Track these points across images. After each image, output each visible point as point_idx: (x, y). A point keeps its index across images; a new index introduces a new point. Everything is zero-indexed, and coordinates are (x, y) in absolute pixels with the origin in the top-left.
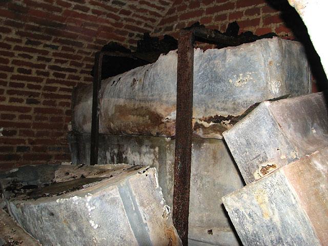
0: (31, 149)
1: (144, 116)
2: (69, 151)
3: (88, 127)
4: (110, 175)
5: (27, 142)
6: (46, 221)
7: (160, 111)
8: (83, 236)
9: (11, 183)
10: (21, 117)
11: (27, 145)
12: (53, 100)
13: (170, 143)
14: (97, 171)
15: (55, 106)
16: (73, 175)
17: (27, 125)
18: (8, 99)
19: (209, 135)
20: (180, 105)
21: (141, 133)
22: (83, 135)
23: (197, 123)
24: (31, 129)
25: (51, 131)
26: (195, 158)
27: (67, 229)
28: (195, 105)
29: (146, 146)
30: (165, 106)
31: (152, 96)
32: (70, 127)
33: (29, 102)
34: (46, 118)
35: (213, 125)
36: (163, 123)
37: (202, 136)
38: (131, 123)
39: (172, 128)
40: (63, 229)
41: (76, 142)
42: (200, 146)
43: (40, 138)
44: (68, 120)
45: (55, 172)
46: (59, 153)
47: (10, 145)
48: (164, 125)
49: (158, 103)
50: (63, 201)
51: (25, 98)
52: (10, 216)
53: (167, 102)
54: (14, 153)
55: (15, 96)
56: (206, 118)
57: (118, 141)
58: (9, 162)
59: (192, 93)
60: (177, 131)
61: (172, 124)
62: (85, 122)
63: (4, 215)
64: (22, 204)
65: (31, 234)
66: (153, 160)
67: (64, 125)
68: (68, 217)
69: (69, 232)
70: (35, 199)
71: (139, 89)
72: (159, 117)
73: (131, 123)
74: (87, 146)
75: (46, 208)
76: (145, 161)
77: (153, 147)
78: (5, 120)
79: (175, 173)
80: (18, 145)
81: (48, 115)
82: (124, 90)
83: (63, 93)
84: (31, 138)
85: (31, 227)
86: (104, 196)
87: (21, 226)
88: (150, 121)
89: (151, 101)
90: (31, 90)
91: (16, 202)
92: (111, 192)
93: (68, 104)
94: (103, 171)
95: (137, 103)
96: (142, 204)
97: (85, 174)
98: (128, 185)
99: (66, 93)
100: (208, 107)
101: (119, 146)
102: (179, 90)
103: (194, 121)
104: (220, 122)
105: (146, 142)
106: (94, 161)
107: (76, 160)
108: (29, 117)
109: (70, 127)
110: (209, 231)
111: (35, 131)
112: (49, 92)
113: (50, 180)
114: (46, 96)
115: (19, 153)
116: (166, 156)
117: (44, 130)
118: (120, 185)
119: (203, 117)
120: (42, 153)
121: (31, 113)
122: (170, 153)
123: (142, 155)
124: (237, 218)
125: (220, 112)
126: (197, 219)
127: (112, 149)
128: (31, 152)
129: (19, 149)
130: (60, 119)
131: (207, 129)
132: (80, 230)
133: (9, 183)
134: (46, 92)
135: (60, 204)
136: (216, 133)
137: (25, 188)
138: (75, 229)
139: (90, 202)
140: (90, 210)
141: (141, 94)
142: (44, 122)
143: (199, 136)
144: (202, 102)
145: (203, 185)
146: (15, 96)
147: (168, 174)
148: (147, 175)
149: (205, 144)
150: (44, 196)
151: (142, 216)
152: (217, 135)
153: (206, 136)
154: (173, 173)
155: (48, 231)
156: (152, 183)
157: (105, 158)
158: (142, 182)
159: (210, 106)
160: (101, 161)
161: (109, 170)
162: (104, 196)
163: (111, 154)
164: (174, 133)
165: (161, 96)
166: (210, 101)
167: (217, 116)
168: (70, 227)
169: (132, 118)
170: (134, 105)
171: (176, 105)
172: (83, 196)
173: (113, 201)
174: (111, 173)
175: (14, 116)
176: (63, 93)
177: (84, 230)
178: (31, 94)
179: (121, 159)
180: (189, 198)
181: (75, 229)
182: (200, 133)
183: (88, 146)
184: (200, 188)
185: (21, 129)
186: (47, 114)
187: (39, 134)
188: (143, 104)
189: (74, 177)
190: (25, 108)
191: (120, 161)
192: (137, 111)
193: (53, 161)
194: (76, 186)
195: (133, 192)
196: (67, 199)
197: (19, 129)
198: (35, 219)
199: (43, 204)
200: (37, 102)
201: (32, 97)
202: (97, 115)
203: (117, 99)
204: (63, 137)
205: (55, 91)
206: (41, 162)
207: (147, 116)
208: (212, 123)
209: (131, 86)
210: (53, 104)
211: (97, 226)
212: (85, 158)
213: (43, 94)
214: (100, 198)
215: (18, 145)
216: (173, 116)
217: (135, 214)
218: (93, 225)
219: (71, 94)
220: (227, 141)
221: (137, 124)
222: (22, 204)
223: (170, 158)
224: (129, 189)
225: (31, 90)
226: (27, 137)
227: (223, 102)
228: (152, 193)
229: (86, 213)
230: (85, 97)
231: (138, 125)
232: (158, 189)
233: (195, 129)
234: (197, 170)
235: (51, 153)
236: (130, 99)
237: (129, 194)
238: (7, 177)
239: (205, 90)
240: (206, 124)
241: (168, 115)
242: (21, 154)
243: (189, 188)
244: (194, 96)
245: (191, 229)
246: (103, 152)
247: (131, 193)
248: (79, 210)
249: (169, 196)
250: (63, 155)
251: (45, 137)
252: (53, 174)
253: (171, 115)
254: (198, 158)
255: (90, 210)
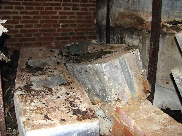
0: (76, 34)
1: (134, 19)
2: (95, 34)
3: (105, 23)
4: (116, 51)
5: (74, 30)
6: (84, 74)
7: (143, 16)
8: (101, 82)
9: (67, 53)
10: (70, 17)
11: (74, 32)
12: (86, 7)
13: (148, 34)
14: (109, 47)
15: (87, 10)
16: (97, 49)
17: (73, 22)
18: (63, 8)
19: (169, 31)
20: (154, 14)
21: (132, 28)
22: (102, 26)
23: (163, 24)
24: (76, 23)
25: (86, 24)
26: (161, 43)
27: (94, 79)
28: (163, 14)
29: (135, 35)
30: (145, 14)
31: (139, 8)
32: (95, 22)
33: (74, 9)
34: (83, 18)
35: (172, 26)
36: (144, 23)
37: (166, 32)
38: (127, 23)
39: (149, 26)
40: (92, 78)
41: (98, 30)
42: (164, 37)
43: (80, 28)
44: (94, 18)
45: (88, 47)
46: (90, 36)
47: (66, 32)
48: (145, 24)
49: (142, 12)
50: (91, 65)
51: (71, 7)
52: (67, 69)
53: (147, 12)
54: (68, 36)
55: (66, 7)
56: (168, 22)
57: (120, 31)
58: (65, 41)
59: (161, 7)
60: (152, 28)
61: (149, 24)
62: (103, 20)
63: (65, 69)
64: (72, 65)
65: (77, 79)
66: (139, 43)
67: (92, 21)
68: (94, 73)
69: (94, 80)
70: (79, 63)
71: (131, 4)
72: (142, 20)
73: (127, 23)
74: (104, 32)
75: (83, 68)
76: (135, 43)
77: (139, 36)
78: (62, 19)
79: (150, 51)
80: (69, 32)
81: (84, 16)
82: (124, 4)
83: (91, 3)
84: (76, 28)
85: (77, 76)
86: (111, 64)
87: (72, 75)
88: (137, 22)
89: (138, 10)
90: (74, 3)
91: (70, 64)
92: (115, 62)
93: (94, 9)
94: (112, 48)
95: (131, 12)
96: (131, 68)
97: (103, 49)
98: (124, 58)
99: (93, 7)
100: (170, 15)
101: (121, 34)
102: (153, 5)
103: (162, 23)
104: (176, 25)
105: (135, 33)
106: (108, 42)
107: (99, 39)
108: (74, 17)
109: (95, 22)
110: (167, 82)
111: (77, 24)
112: (83, 3)
113: (86, 51)
114: (82, 5)
115: (70, 36)
116: (146, 41)
117: (82, 23)
118: (120, 59)
119: (167, 21)
120: (81, 35)
121: (75, 15)
122: (148, 40)
123: (133, 39)
124: (178, 81)
125: (177, 19)
126: (161, 75)
127: (117, 35)
128: (76, 35)
129: (70, 34)
130: (90, 18)
131: (169, 28)
132: (100, 80)
133: (66, 52)
134: (82, 3)
135: (90, 67)
136: (174, 30)
137: (74, 55)
138: (97, 79)
139: (104, 67)
140: (104, 71)
141: (132, 6)
142: (82, 19)
143: (164, 32)
144: (167, 12)
145: (165, 58)
146: (66, 7)
147: (146, 50)
148: (134, 54)
149: (167, 36)
150: (83, 61)
151: (131, 74)
152: (174, 31)
153: (168, 32)
154: (149, 51)
155: (85, 79)
156: (137, 58)
157: (114, 39)
158: (131, 57)
159: (171, 14)
160: (112, 41)
161: (115, 47)
162: (111, 64)
163: (117, 38)
164: (150, 29)
165: (143, 8)
166: (171, 12)
167: (175, 21)
168: (95, 78)
169: (128, 20)
170: (129, 13)
171: (152, 14)
172: (101, 63)
173: (116, 66)
174: (116, 49)
175: (66, 17)
176: (91, 3)
177: (102, 80)
178: (74, 5)
179: (122, 41)
180: (157, 64)
181: (97, 79)
182: (165, 30)
183: (105, 32)
184: (163, 59)
185: (70, 23)
186: (83, 15)
187: (80, 26)
188: (133, 12)
189: (97, 50)
190: (72, 12)
191: (121, 43)
192: (130, 16)
193: (87, 39)
194: (98, 56)
195: (126, 62)
196: (93, 65)
197: (69, 24)
198: (79, 73)
199: (82, 66)
200: (77, 9)
201: (75, 7)
202: (109, 17)
203: (119, 9)
204: (92, 27)
205: (87, 3)
206: (81, 40)
207: (136, 19)
208: (171, 25)
209: (127, 2)
210: (86, 9)
211: (108, 78)
212: (104, 39)
213: (80, 5)
214: (110, 65)
215: (69, 32)
216: (150, 19)
217: (127, 73)
218: (106, 78)
219: (95, 4)
220: (177, 38)
221: (130, 23)
222: (72, 65)
223: (148, 42)
224: (124, 60)
225: (74, 3)
226: (74, 28)
227: (179, 13)
228: (136, 63)
229: (102, 72)
230: (103, 7)
231: (131, 24)
232: (140, 61)
233: (162, 28)
234: (162, 49)
235: (86, 35)
236: (127, 9)
237: (124, 63)
238: (65, 49)
239: (169, 5)
240: (168, 25)
241: (147, 19)
242: (71, 36)
243: (157, 59)
244: (162, 9)
245: (157, 81)
246: (112, 37)
247: (125, 63)
248: (99, 70)
249: (147, 62)
250: (92, 36)
251: (83, 27)
252: (87, 48)
253: (149, 19)
254: (163, 43)
255: (104, 71)
